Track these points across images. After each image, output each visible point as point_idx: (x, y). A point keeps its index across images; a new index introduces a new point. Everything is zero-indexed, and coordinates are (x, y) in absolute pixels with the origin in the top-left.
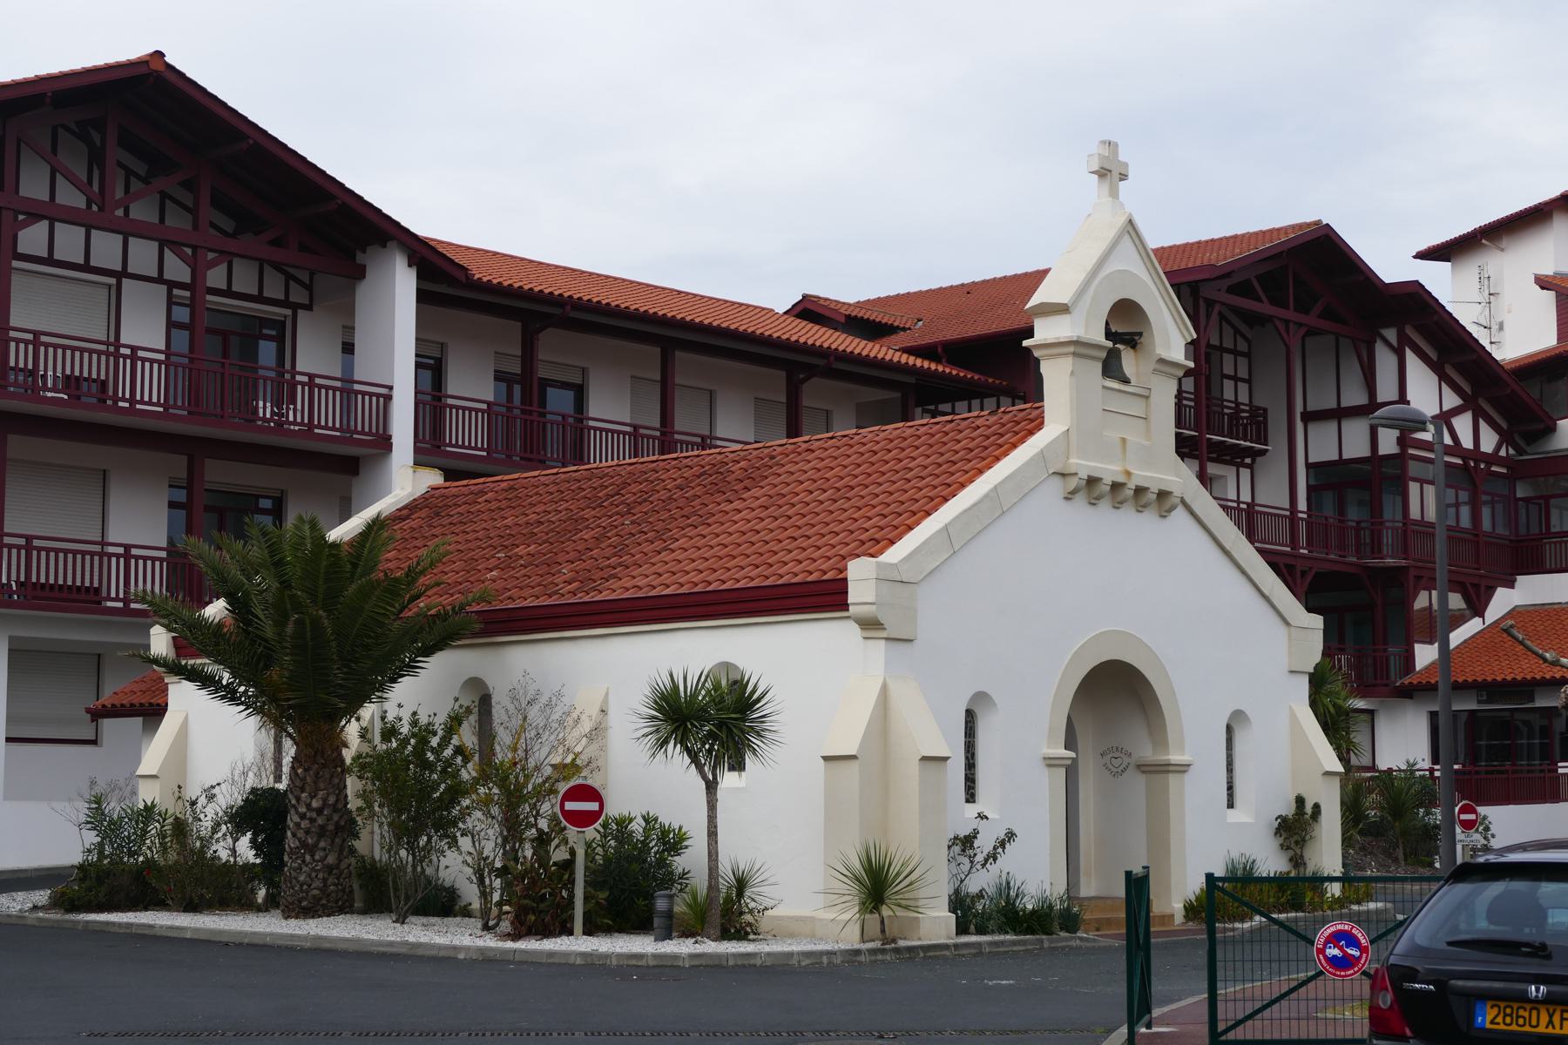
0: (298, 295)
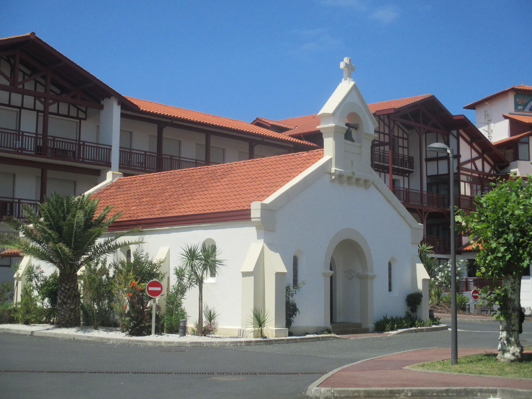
0: (81, 115)
